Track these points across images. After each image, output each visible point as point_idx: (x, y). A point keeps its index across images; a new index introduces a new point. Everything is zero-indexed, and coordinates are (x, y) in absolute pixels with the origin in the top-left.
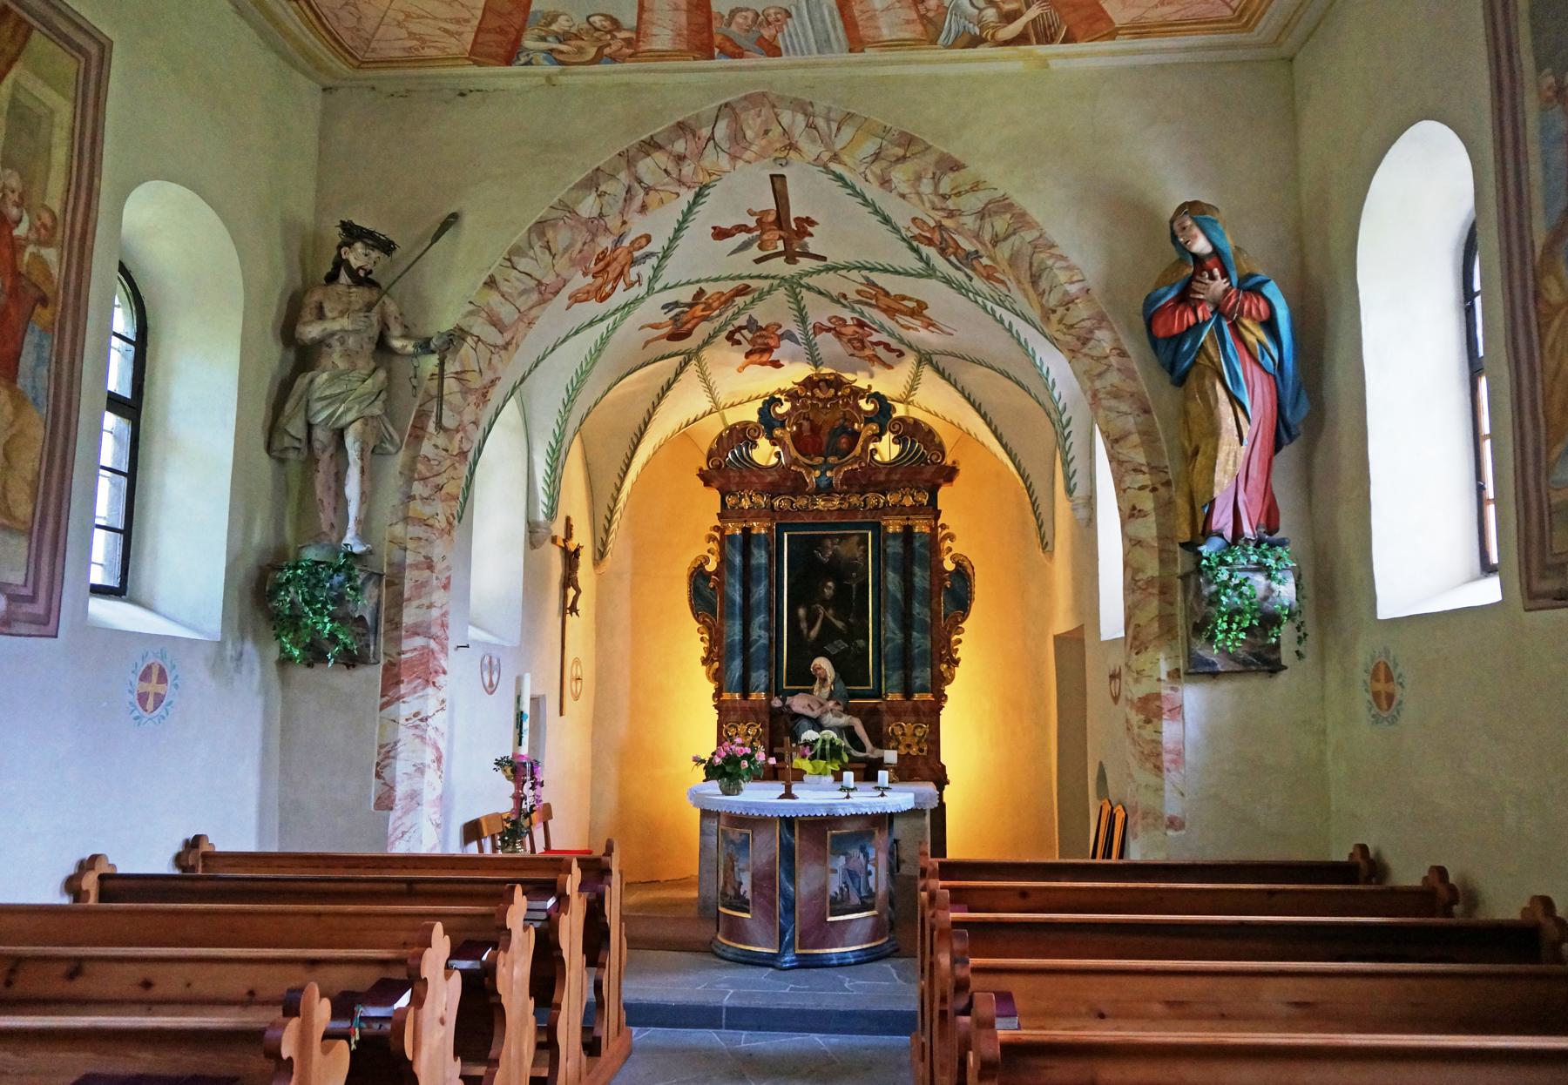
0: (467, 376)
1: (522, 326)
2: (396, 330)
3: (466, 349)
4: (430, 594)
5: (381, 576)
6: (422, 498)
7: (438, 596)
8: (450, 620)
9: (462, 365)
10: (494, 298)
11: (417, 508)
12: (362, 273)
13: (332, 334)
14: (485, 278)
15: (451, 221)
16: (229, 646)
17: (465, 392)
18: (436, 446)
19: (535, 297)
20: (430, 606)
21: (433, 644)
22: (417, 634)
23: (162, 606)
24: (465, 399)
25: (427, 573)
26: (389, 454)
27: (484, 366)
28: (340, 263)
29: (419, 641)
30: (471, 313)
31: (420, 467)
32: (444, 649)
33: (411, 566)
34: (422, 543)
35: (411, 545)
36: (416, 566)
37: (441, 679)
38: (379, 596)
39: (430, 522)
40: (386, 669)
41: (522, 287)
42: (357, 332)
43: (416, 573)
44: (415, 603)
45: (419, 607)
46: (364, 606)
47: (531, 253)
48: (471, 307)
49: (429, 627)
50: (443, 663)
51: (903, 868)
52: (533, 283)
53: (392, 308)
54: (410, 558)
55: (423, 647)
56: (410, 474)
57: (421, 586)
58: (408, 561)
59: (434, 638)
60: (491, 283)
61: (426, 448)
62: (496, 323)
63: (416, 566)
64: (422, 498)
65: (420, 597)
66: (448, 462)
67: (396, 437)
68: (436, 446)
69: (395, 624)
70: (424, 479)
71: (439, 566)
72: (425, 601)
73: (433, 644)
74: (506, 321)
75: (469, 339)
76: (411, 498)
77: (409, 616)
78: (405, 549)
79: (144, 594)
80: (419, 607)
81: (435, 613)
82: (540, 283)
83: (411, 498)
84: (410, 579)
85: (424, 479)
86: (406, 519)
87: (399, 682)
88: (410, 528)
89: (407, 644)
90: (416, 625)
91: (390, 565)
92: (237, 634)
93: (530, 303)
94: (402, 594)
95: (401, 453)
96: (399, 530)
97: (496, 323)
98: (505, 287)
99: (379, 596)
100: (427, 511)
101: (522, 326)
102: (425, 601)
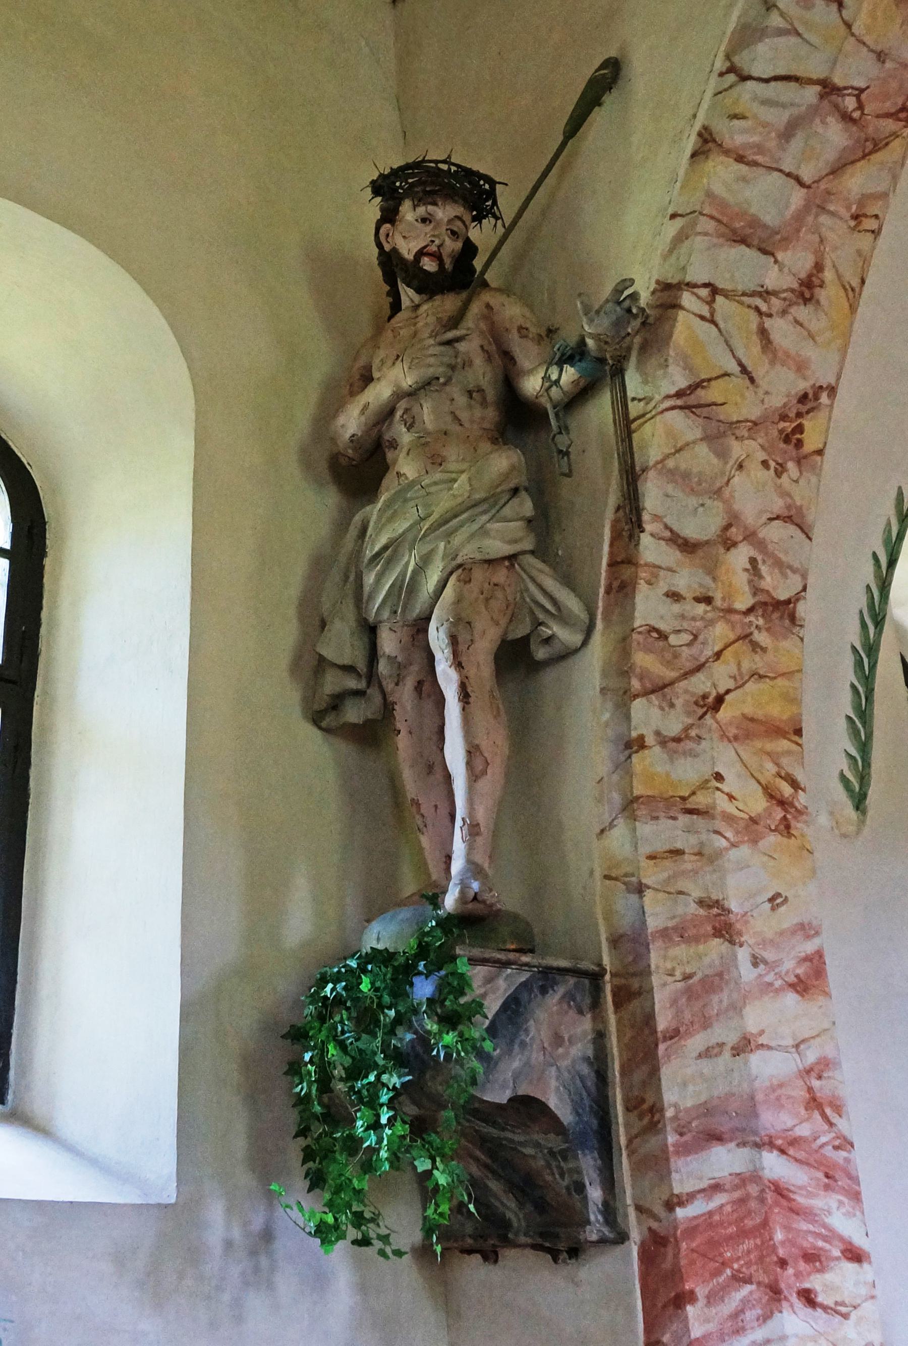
0: (713, 393)
1: (834, 228)
2: (526, 354)
3: (686, 327)
4: (736, 1009)
5: (595, 977)
6: (663, 741)
7: (775, 1016)
8: (848, 1082)
9: (688, 367)
10: (720, 173)
11: (651, 763)
12: (429, 265)
13: (387, 413)
14: (690, 143)
15: (608, 77)
16: (215, 1212)
17: (719, 434)
18: (674, 596)
19: (834, 136)
20: (745, 1046)
21: (774, 1166)
22: (717, 1137)
23: (68, 1123)
24: (722, 454)
25: (716, 947)
26: (567, 654)
27: (751, 354)
28: (392, 265)
29: (724, 1161)
30: (680, 238)
31: (643, 660)
32: (837, 1177)
33: (664, 934)
34: (689, 863)
35: (651, 875)
36: (679, 933)
37: (838, 1281)
38: (600, 1037)
39: (701, 800)
40: (648, 1258)
41: (779, 118)
42: (426, 385)
43: (680, 951)
44: (696, 1042)
45: (707, 1054)
46: (546, 1063)
47: (775, 20)
48: (679, 222)
49: (751, 1108)
50: (843, 1223)
51: (733, 530)
52: (811, 93)
53: (512, 311)
54: (657, 913)
55: (742, 1180)
56: (622, 692)
57: (701, 989)
58: (653, 924)
59: (785, 1146)
60: (707, 144)
61: (648, 607)
62: (744, 233)
63: (679, 933)
64: (663, 741)
65: (706, 1024)
66: (720, 632)
67: (572, 603)
68: (674, 596)
69: (648, 1112)
70: (659, 688)
71: (760, 925)
72: (724, 1033)
73: (774, 1166)
74: (770, 218)
75: (687, 299)
76: (634, 745)
77: (682, 1085)
78: (640, 889)
79: (37, 1107)
80: (707, 1054)
81: (767, 1067)
82: (829, 89)
83: (634, 745)
84: (666, 972)
85: (659, 688)
86: (630, 806)
87: (682, 1299)
88: (645, 829)
89: (692, 1172)
90: (707, 1110)
91: (615, 941)
92: (245, 1179)
93: (830, 155)
94: (649, 1019)
95: (597, 637)
96: (619, 839)
97: (744, 233)
98: (737, 135)
99: (600, 1037)
100: (686, 772)
101: (834, 228)
102: (724, 1033)
